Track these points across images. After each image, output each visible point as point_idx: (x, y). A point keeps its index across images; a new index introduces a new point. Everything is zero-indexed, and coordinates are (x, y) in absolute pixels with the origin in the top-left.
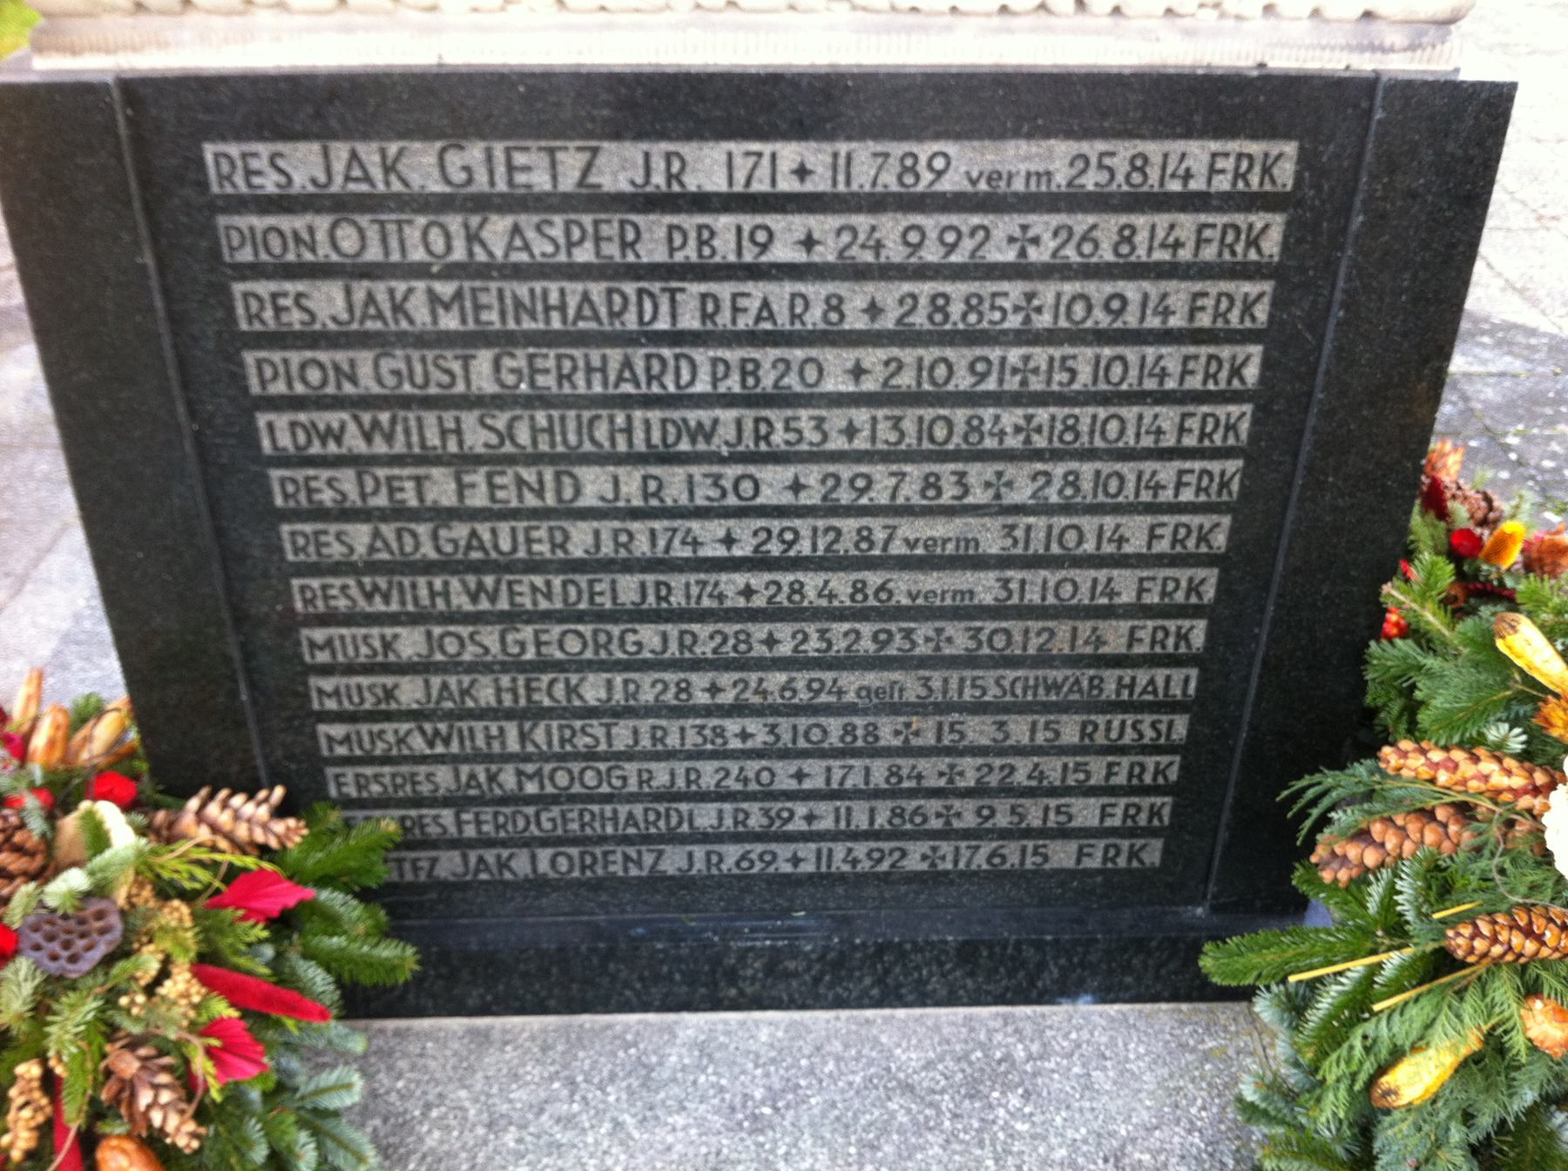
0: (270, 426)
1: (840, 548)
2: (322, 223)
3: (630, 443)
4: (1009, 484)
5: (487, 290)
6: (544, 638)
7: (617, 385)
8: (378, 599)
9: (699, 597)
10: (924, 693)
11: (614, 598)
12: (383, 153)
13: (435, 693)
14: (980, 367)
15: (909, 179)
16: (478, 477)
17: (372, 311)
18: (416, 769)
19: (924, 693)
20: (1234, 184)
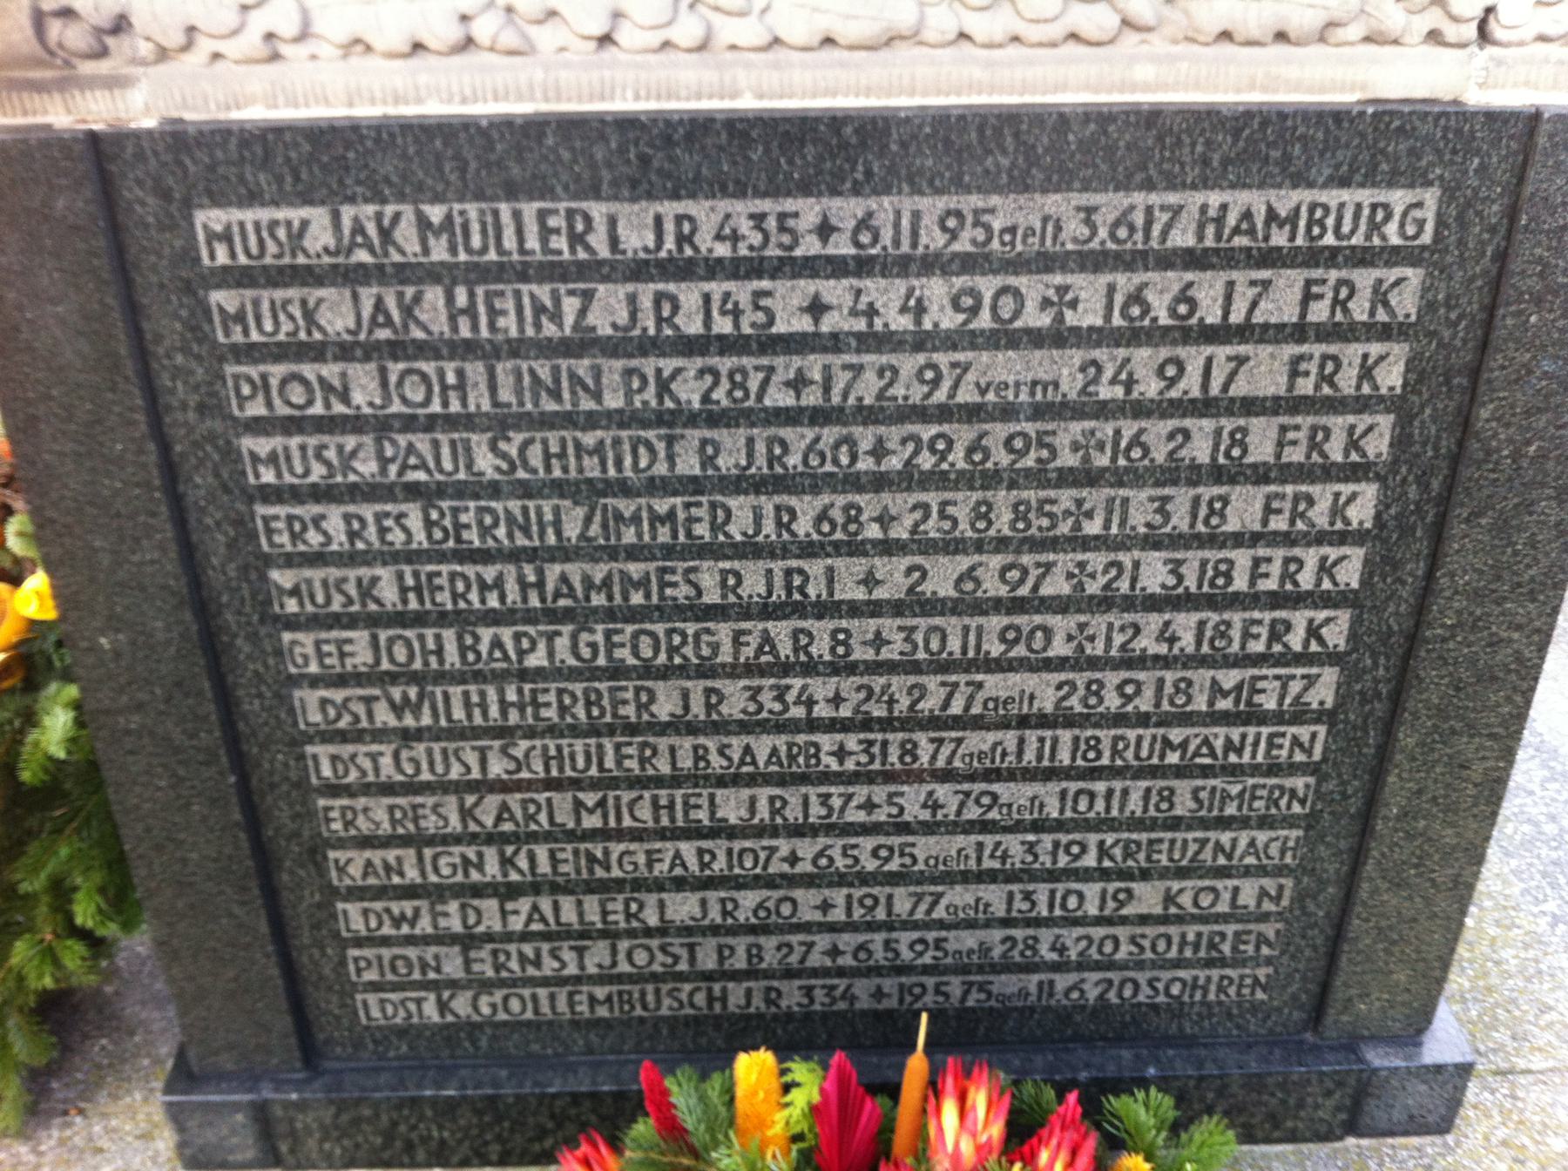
0: (365, 1003)
3: (673, 819)
4: (1073, 304)
6: (616, 639)
9: (842, 810)
10: (1171, 581)
11: (713, 813)
12: (400, 295)
14: (1018, 444)
15: (865, 238)
16: (453, 907)
17: (381, 319)
19: (1171, 581)
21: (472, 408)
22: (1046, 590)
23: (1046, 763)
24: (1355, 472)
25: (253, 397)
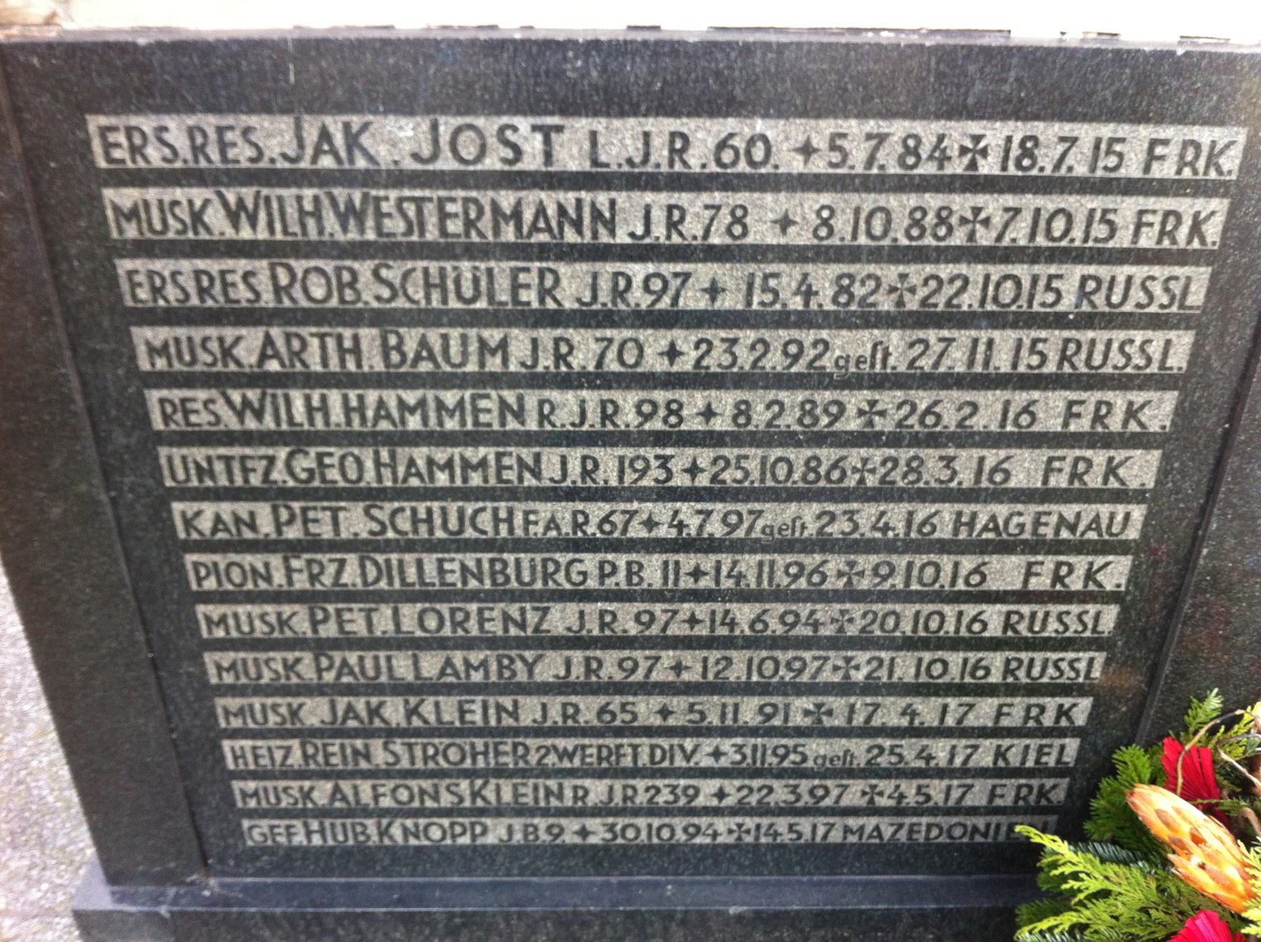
0: (170, 459)
1: (781, 422)
2: (276, 560)
5: (387, 199)
7: (530, 235)
8: (249, 416)
13: (340, 713)
18: (229, 263)
20: (1159, 241)
21: (366, 369)
22: (655, 677)
23: (978, 369)
24: (1142, 440)
25: (208, 575)
